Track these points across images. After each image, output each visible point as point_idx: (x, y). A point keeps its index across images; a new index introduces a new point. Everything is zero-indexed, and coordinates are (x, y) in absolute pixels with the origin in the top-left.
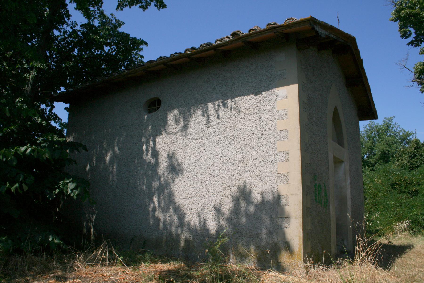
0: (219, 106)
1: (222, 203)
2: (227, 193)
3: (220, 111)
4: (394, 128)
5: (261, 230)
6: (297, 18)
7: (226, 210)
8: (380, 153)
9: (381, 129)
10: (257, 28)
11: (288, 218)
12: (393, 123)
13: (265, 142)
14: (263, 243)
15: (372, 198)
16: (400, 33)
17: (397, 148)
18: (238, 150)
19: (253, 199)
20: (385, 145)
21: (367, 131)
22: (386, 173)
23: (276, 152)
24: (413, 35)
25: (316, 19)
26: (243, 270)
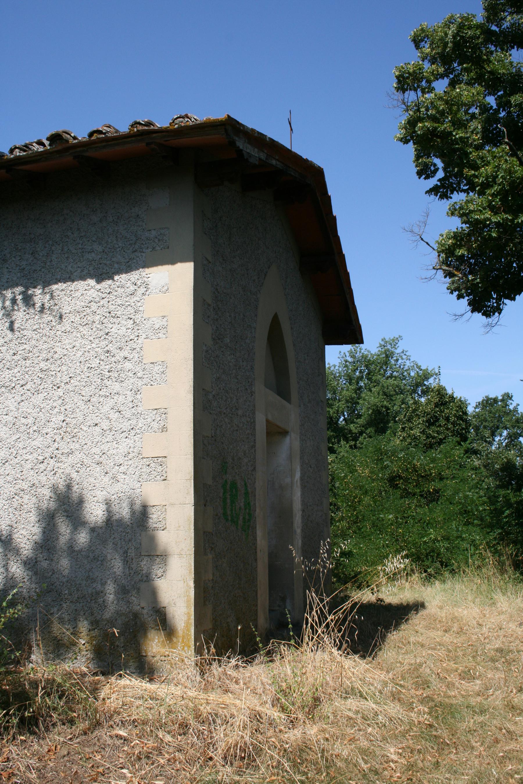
0: (14, 301)
1: (15, 526)
2: (26, 501)
3: (16, 313)
4: (400, 361)
5: (104, 584)
6: (199, 115)
7: (25, 540)
8: (370, 412)
9: (373, 362)
10: (108, 129)
11: (164, 557)
12: (399, 351)
13: (117, 387)
14: (108, 615)
15: (350, 506)
16: (416, 166)
17: (403, 403)
18: (55, 404)
19: (88, 516)
20: (381, 397)
21: (346, 366)
22: (380, 455)
23: (140, 409)
24: (440, 174)
25: (238, 122)
26: (59, 680)
